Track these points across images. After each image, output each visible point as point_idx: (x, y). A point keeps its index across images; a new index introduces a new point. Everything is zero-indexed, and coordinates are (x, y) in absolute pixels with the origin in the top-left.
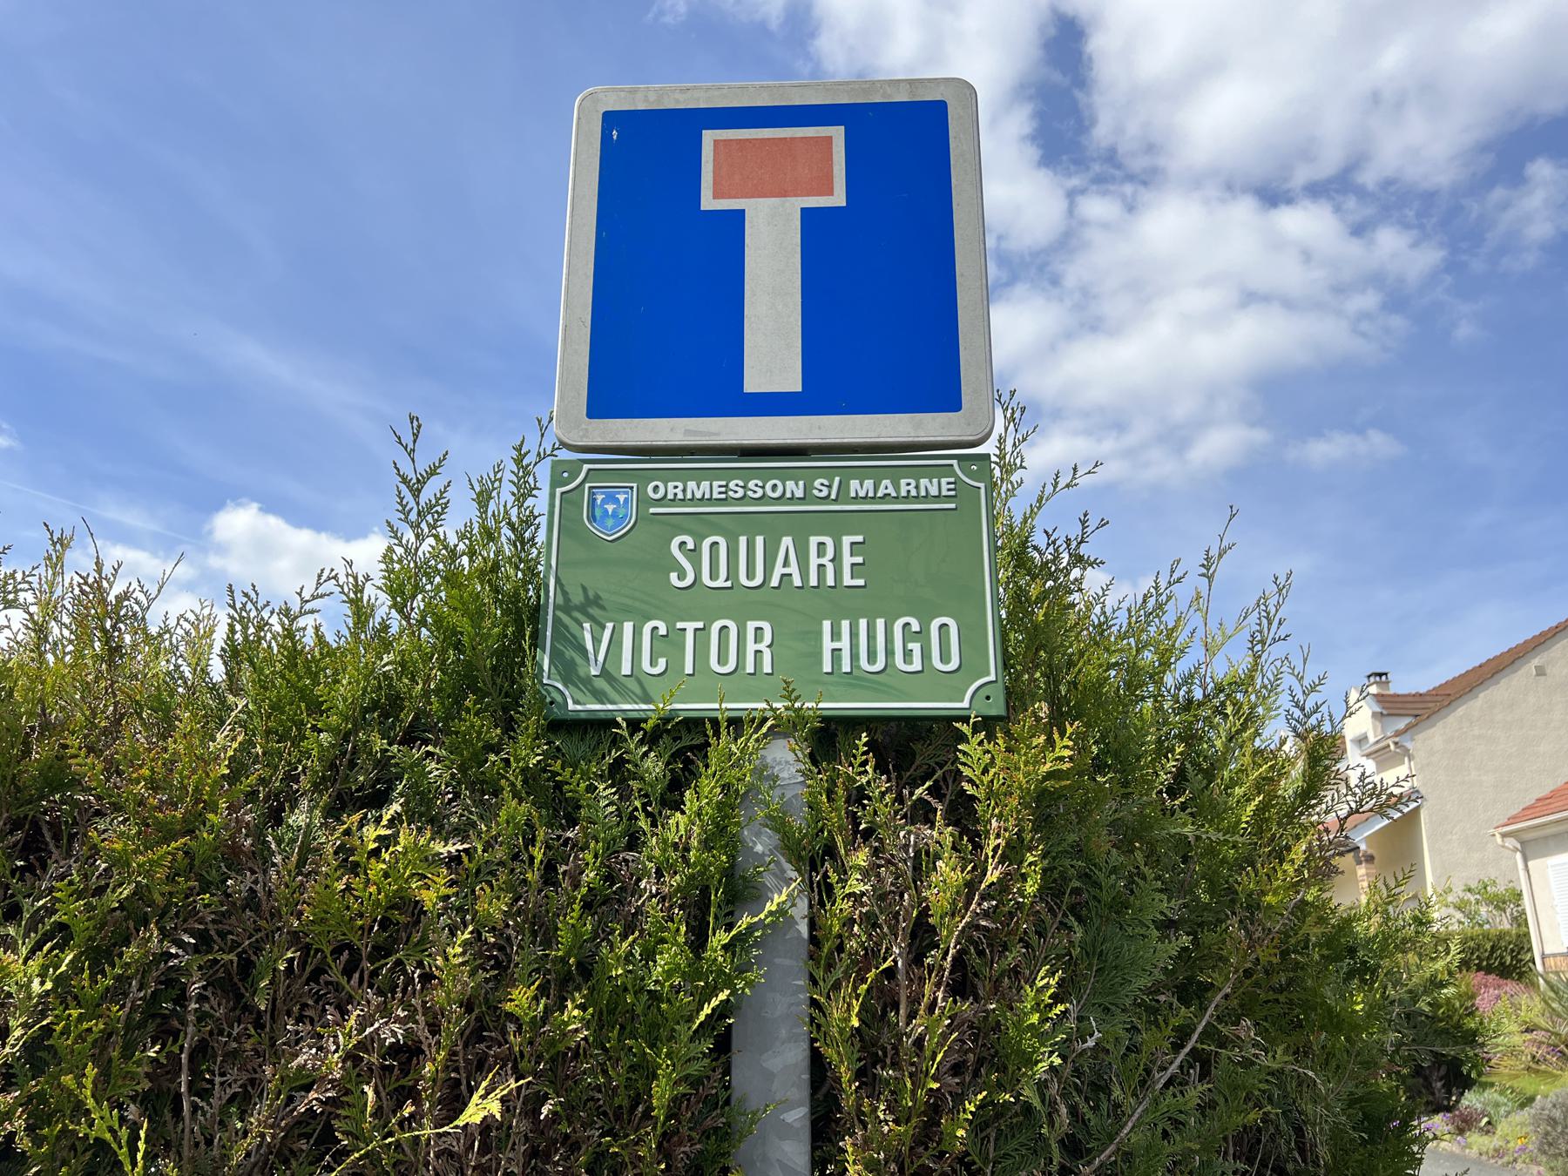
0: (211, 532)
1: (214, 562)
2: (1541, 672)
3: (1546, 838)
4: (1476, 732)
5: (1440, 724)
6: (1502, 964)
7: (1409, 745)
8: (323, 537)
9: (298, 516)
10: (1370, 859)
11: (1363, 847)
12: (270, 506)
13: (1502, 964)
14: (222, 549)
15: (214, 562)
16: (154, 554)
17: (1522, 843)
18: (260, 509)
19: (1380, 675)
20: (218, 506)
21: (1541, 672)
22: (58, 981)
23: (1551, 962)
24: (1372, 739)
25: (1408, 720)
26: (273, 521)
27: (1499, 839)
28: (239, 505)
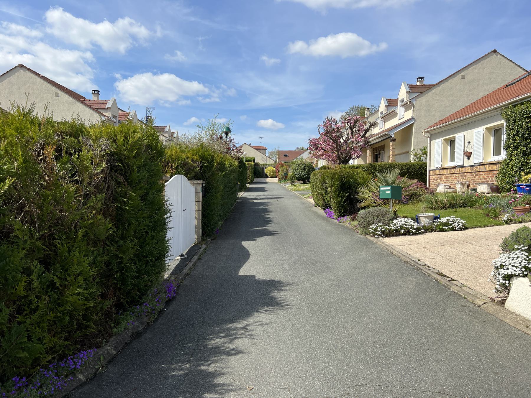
0: (45, 19)
1: (48, 30)
2: (463, 77)
3: (437, 133)
4: (437, 98)
5: (426, 95)
6: (421, 173)
7: (414, 103)
8: (87, 22)
9: (78, 13)
10: (394, 140)
11: (393, 136)
12: (67, 9)
13: (421, 173)
14: (51, 26)
15: (48, 30)
16: (27, 27)
17: (431, 135)
18: (63, 10)
19: (421, 78)
20: (48, 8)
21: (463, 77)
22: (507, 148)
23: (431, 172)
24: (405, 101)
25: (419, 94)
26: (68, 15)
27: (424, 134)
28: (54, 8)
